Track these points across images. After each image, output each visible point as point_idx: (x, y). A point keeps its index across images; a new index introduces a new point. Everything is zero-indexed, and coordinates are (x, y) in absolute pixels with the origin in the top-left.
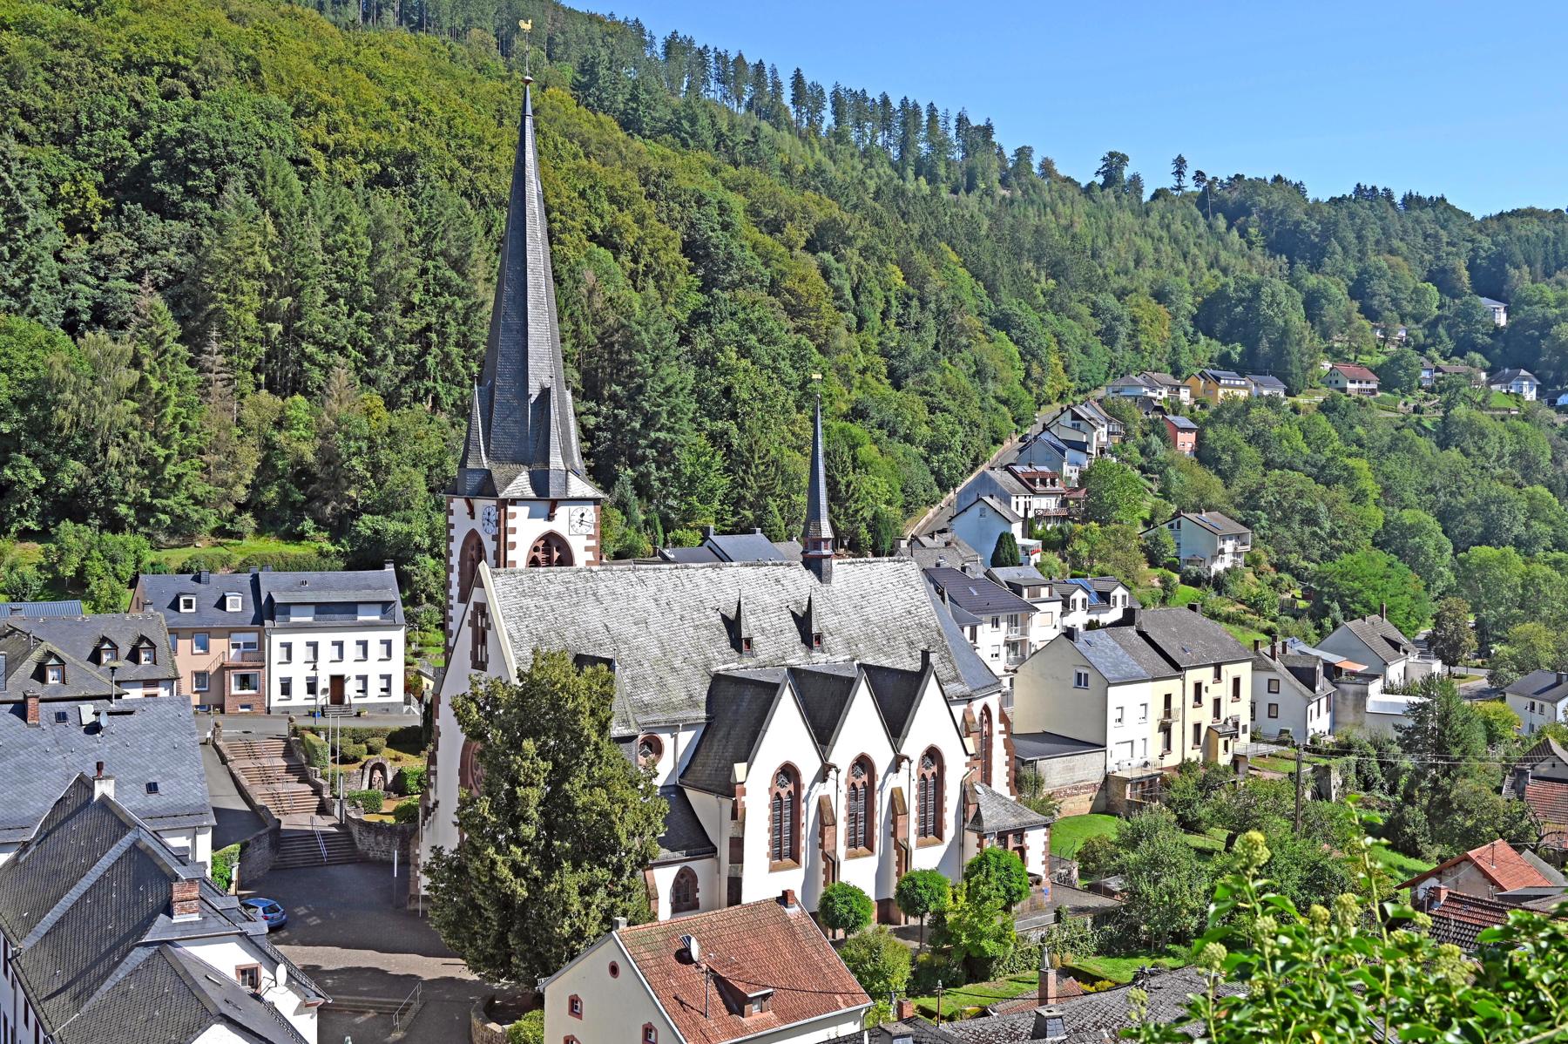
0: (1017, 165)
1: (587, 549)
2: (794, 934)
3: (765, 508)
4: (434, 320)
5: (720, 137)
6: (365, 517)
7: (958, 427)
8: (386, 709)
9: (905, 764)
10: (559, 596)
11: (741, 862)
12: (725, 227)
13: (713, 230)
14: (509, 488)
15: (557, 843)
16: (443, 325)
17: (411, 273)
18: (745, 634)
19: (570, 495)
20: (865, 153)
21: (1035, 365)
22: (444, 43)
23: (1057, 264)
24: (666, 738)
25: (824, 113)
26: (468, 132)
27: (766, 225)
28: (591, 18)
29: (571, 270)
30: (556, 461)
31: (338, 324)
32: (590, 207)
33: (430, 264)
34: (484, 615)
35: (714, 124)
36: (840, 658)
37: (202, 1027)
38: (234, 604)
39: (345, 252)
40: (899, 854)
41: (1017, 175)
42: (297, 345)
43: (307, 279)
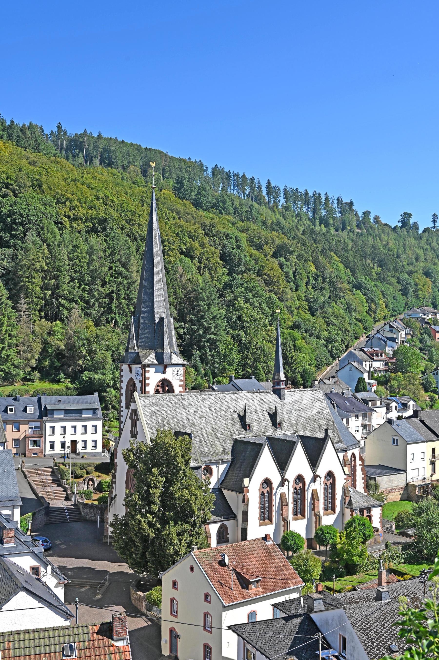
0: (364, 219)
1: (180, 386)
2: (270, 554)
3: (256, 367)
4: (115, 289)
5: (236, 209)
6: (86, 373)
7: (340, 332)
10: (168, 406)
11: (247, 521)
12: (238, 247)
13: (233, 249)
16: (119, 291)
17: (105, 269)
19: (173, 363)
21: (373, 305)
23: (382, 261)
24: (214, 468)
25: (280, 198)
26: (129, 209)
28: (181, 160)
29: (173, 267)
30: (166, 348)
32: (181, 240)
33: (113, 265)
34: (136, 414)
38: (30, 410)
39: (78, 260)
40: (316, 518)
41: (364, 223)
43: (61, 272)
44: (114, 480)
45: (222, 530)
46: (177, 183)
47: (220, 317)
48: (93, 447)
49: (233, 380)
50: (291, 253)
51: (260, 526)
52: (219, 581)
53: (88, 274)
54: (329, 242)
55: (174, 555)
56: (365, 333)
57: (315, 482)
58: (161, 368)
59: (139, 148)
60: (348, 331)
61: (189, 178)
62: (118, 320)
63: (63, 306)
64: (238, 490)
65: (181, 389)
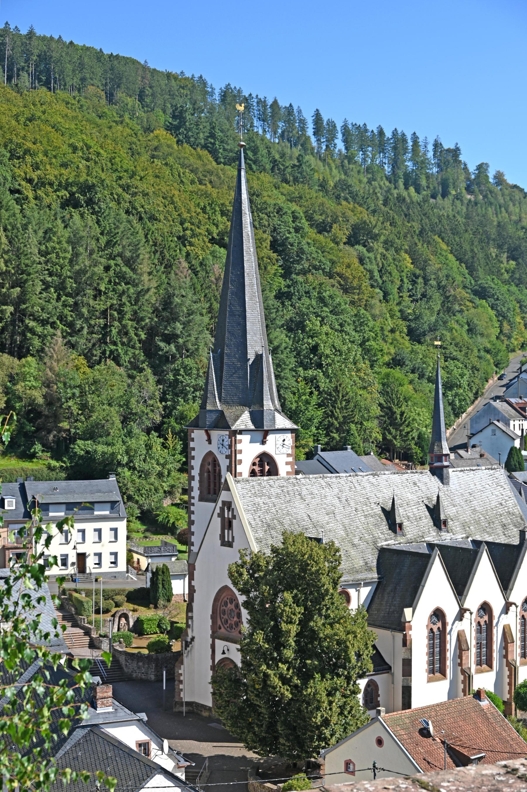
0: (478, 176)
1: (287, 463)
2: (488, 719)
3: (348, 431)
4: (115, 302)
5: (274, 162)
6: (79, 442)
7: (466, 371)
8: (114, 576)
9: (467, 615)
10: (278, 496)
11: (410, 675)
12: (297, 230)
13: (290, 233)
14: (238, 422)
15: (309, 662)
16: (121, 305)
17: (99, 270)
18: (398, 521)
19: (277, 426)
20: (368, 170)
21: (505, 324)
22: (74, 98)
23: (516, 249)
24: (352, 592)
25: (336, 141)
26: (125, 167)
27: (317, 227)
28: (169, 76)
29: (201, 264)
30: (268, 404)
31: (50, 307)
32: (209, 218)
33: (112, 262)
35: (269, 153)
36: (459, 537)
37: (149, 776)
38: (10, 504)
39: (54, 255)
40: (510, 670)
41: (479, 184)
42: (22, 321)
43: (29, 274)
44: (190, 614)
45: (369, 689)
46: (174, 117)
47: (285, 348)
48: (112, 563)
49: (319, 452)
50: (375, 237)
51: (428, 682)
52: (424, 759)
53: (71, 278)
54: (428, 217)
55: (321, 726)
56: (496, 373)
57: (507, 613)
58: (260, 435)
59: (99, 55)
60: (478, 370)
61: (194, 109)
62: (122, 355)
63: (32, 331)
64: (394, 627)
65: (289, 468)
